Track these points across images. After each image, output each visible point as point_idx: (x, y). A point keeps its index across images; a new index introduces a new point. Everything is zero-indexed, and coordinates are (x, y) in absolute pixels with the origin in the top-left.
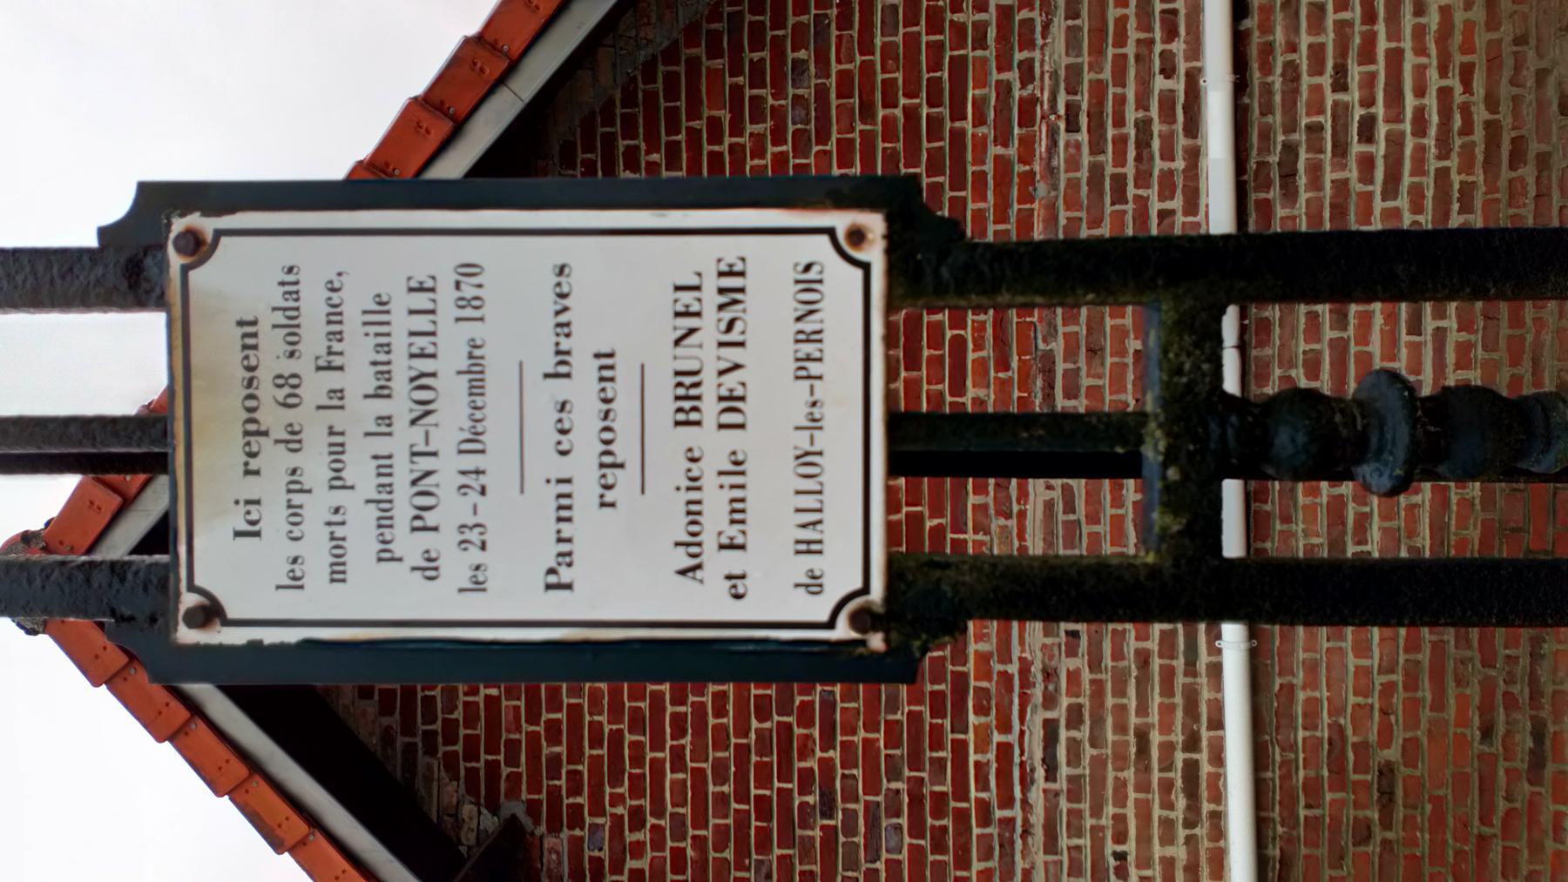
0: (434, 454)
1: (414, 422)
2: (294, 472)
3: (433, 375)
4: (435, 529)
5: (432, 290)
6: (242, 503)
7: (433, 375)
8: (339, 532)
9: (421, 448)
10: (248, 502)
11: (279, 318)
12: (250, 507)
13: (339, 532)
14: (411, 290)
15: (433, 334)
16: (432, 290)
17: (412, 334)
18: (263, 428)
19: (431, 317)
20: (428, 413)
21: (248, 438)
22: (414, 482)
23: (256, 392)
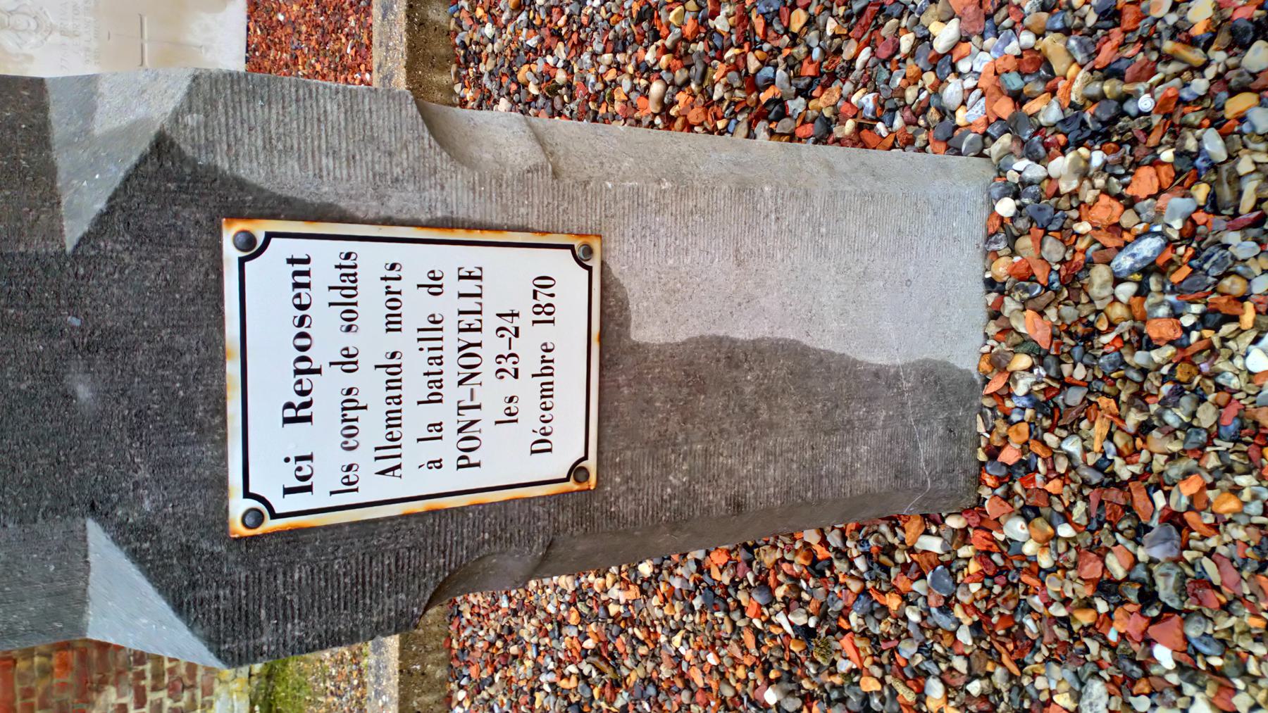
0: (479, 407)
1: (460, 383)
2: (349, 391)
3: (479, 345)
4: (478, 465)
5: (480, 278)
6: (292, 460)
7: (479, 345)
8: (395, 286)
9: (468, 403)
10: (298, 459)
11: (336, 296)
12: (300, 464)
13: (395, 286)
14: (461, 278)
15: (480, 313)
16: (480, 278)
17: (461, 313)
18: (315, 366)
19: (478, 299)
20: (473, 375)
21: (299, 377)
22: (460, 431)
23: (307, 331)
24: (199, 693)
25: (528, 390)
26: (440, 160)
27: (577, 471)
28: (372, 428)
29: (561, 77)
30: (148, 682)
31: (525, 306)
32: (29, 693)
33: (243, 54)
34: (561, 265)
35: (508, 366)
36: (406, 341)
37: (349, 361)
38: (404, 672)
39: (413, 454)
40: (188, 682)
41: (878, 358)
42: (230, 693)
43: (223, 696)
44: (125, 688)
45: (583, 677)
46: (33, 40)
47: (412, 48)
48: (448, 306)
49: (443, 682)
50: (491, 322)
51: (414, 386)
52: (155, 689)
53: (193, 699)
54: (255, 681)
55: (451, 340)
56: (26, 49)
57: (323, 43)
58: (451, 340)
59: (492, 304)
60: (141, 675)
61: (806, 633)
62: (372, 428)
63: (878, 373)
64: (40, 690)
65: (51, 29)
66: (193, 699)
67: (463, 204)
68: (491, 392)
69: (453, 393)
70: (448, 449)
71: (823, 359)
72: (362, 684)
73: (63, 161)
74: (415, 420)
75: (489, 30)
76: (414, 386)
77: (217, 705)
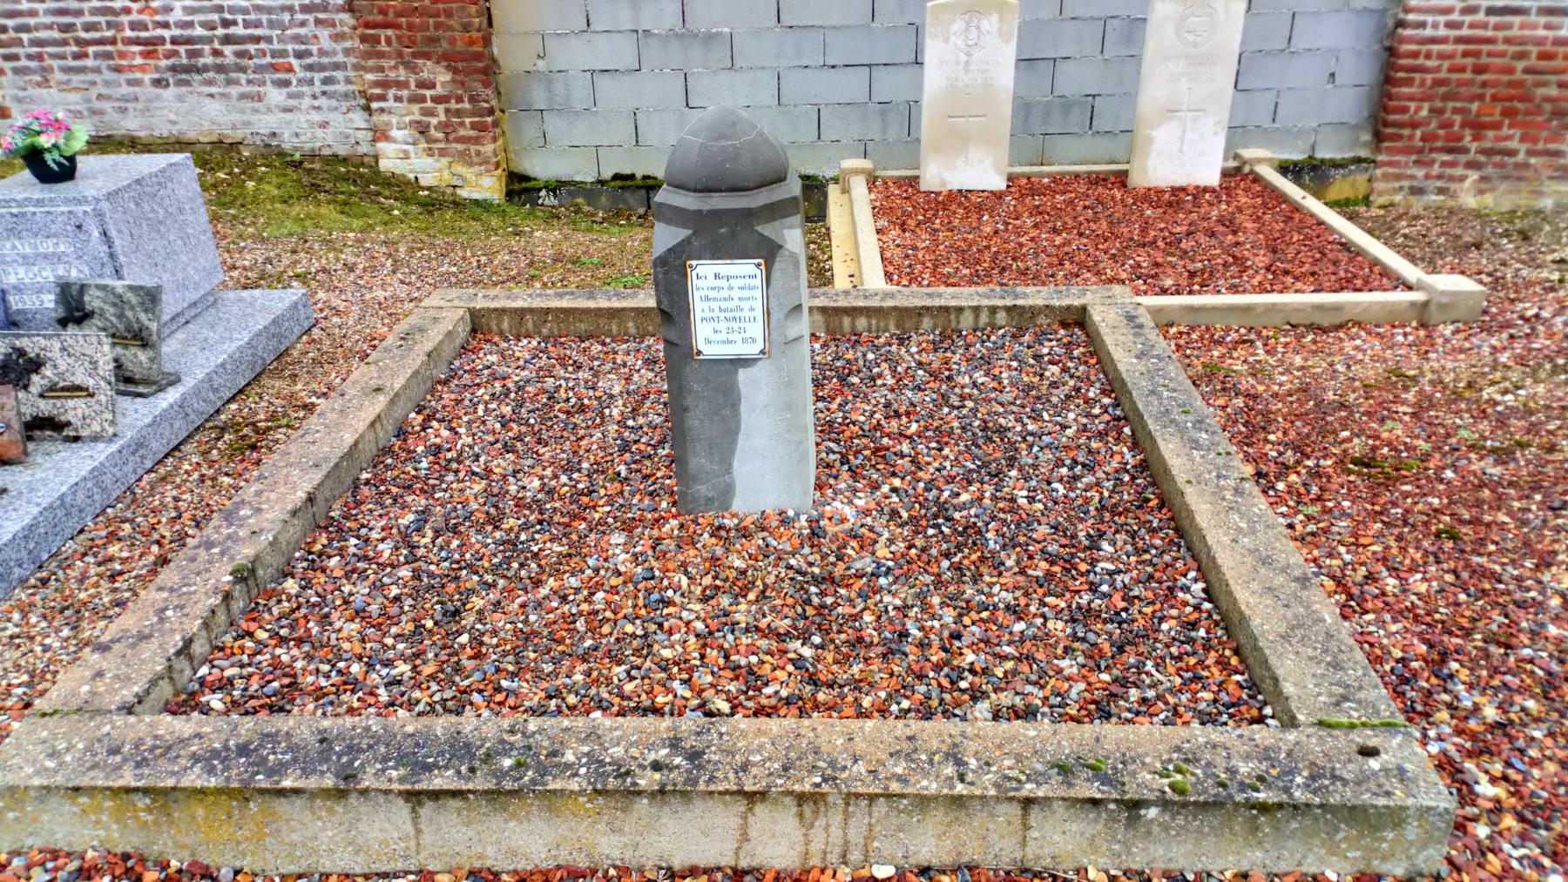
24: (442, 145)
25: (723, 337)
26: (786, 311)
27: (699, 353)
28: (712, 294)
29: (879, 382)
30: (453, 105)
31: (747, 335)
32: (449, 14)
33: (965, 188)
34: (759, 346)
35: (730, 330)
36: (736, 302)
37: (731, 288)
38: (548, 311)
39: (706, 305)
40: (451, 137)
41: (736, 464)
42: (440, 170)
43: (438, 165)
44: (449, 88)
45: (568, 400)
46: (960, 43)
47: (906, 309)
48: (746, 313)
49: (539, 334)
50: (742, 325)
51: (724, 305)
52: (447, 111)
53: (436, 141)
54: (449, 191)
55: (737, 314)
56: (953, 39)
57: (958, 250)
58: (737, 314)
59: (747, 325)
60: (459, 100)
61: (619, 474)
62: (712, 294)
63: (730, 465)
64: (451, 22)
65: (968, 54)
66: (436, 141)
67: (774, 317)
68: (722, 326)
69: (722, 315)
70: (707, 314)
71: (734, 441)
72: (495, 284)
73: (777, 223)
74: (715, 305)
75: (914, 349)
76: (724, 305)
77: (430, 160)
